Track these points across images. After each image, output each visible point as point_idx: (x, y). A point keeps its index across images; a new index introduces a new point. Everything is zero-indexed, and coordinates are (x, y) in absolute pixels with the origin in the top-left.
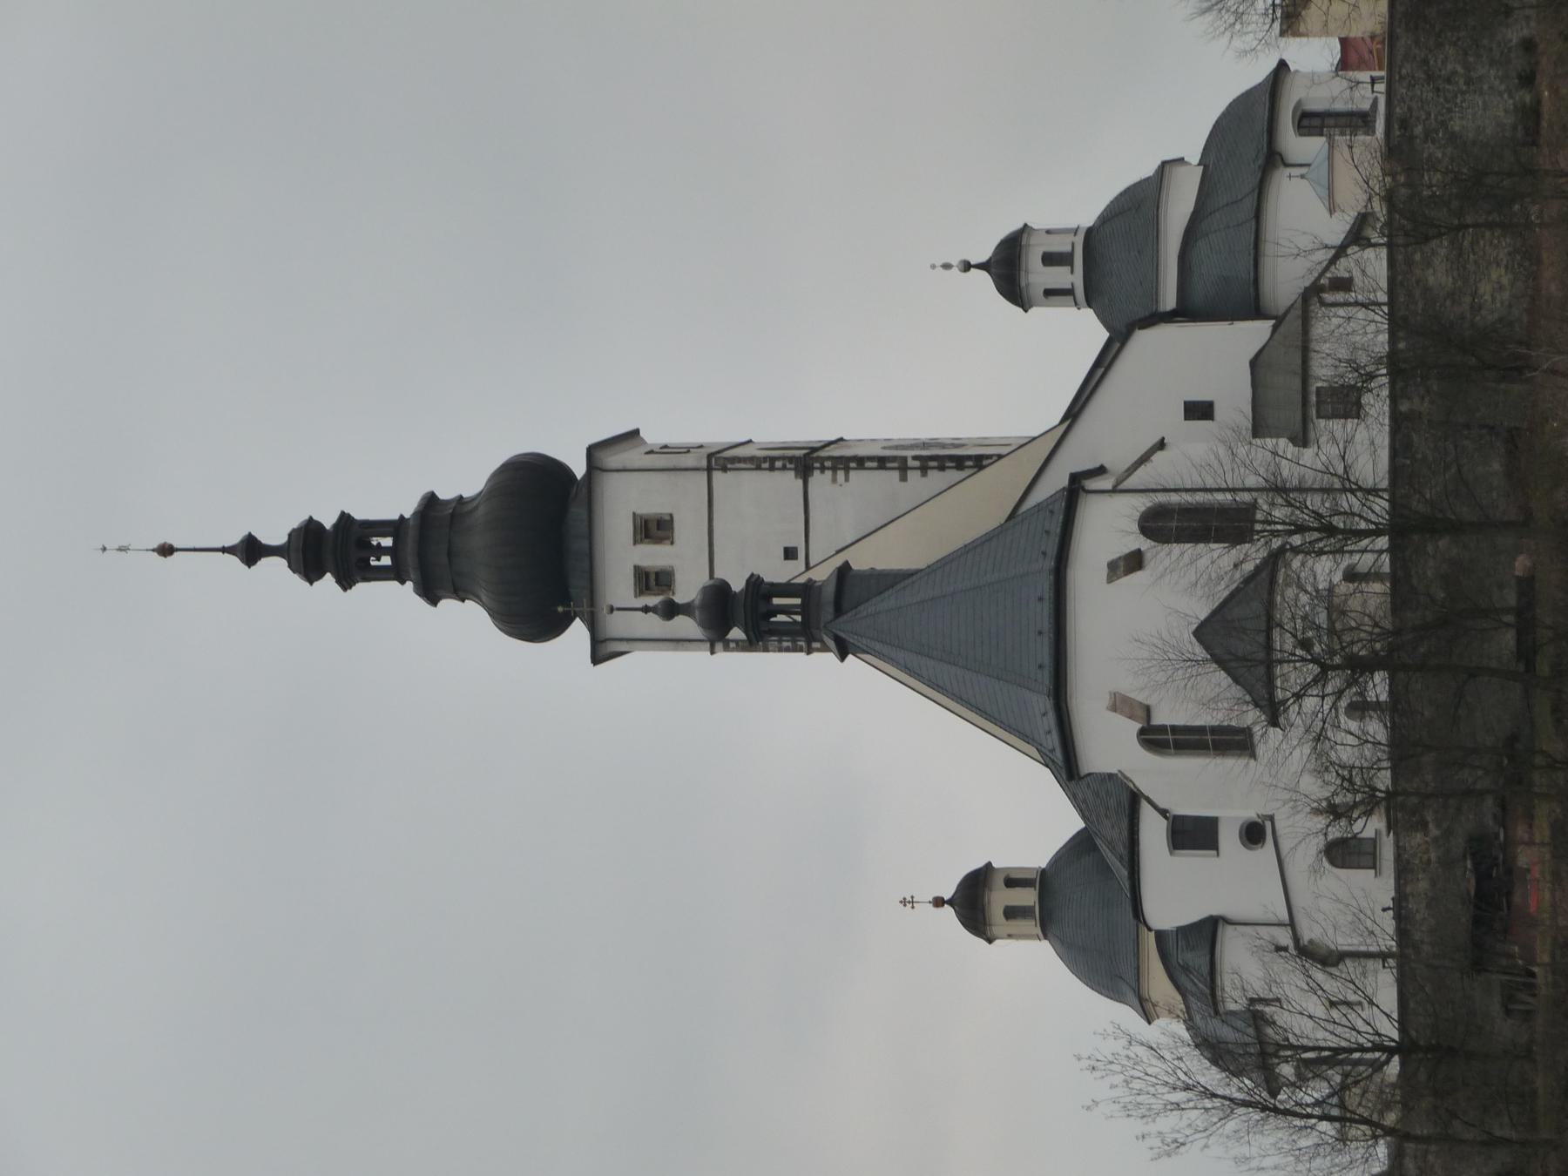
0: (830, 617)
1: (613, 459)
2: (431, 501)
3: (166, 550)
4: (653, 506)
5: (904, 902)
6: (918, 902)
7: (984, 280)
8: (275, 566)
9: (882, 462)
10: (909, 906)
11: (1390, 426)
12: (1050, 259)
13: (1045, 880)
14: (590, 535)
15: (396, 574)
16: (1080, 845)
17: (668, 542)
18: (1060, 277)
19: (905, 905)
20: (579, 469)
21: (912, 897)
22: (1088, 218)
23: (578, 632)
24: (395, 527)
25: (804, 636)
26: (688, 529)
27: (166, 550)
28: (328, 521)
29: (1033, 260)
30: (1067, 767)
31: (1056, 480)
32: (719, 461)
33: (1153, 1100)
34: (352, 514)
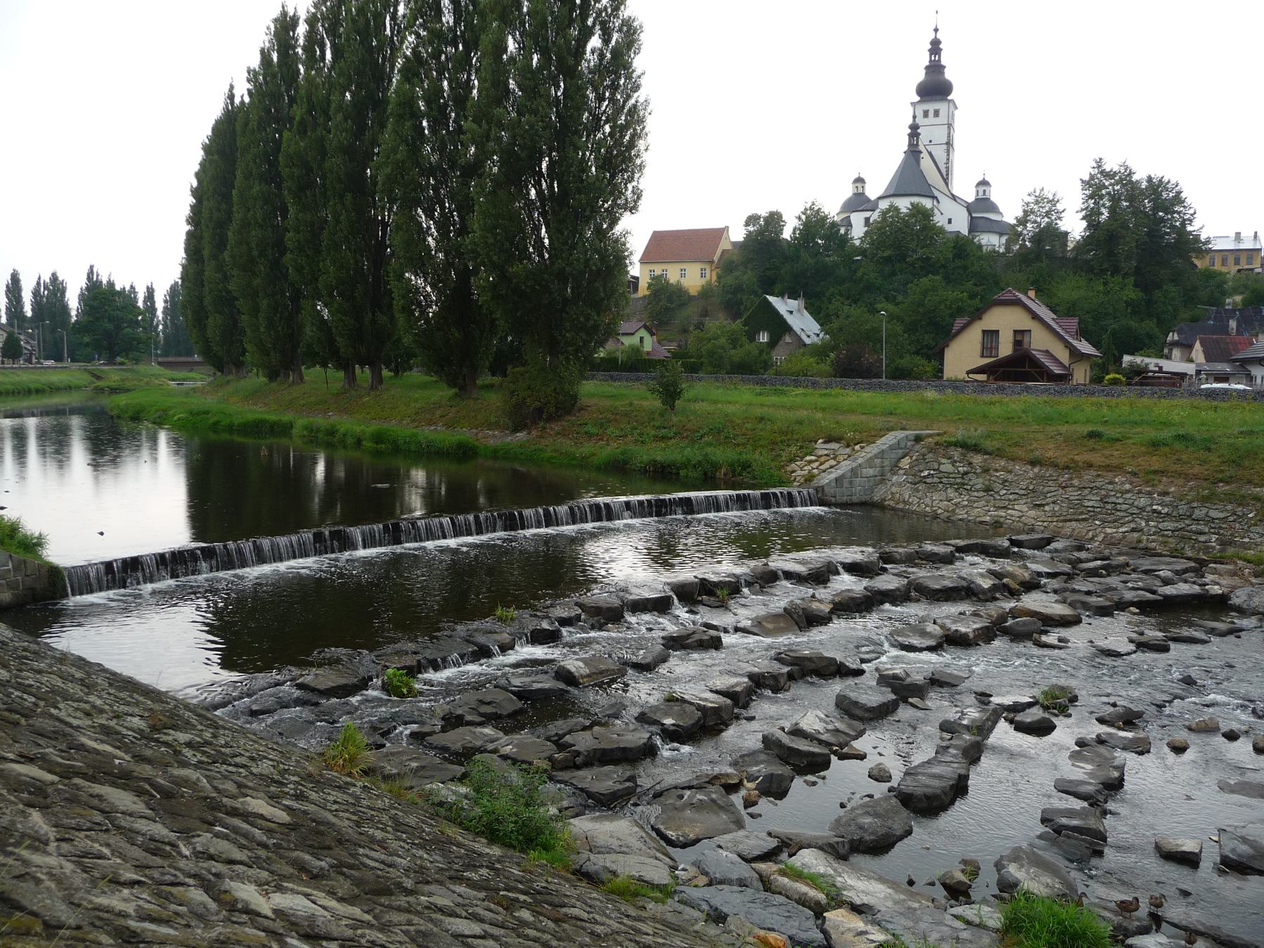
4: (941, 113)
7: (981, 179)
8: (933, 36)
9: (948, 159)
14: (936, 100)
15: (931, 61)
16: (868, 200)
18: (981, 193)
20: (949, 98)
22: (992, 199)
23: (918, 99)
24: (939, 60)
25: (910, 145)
26: (937, 121)
29: (984, 188)
32: (950, 126)
33: (1245, 653)
34: (187, 211)
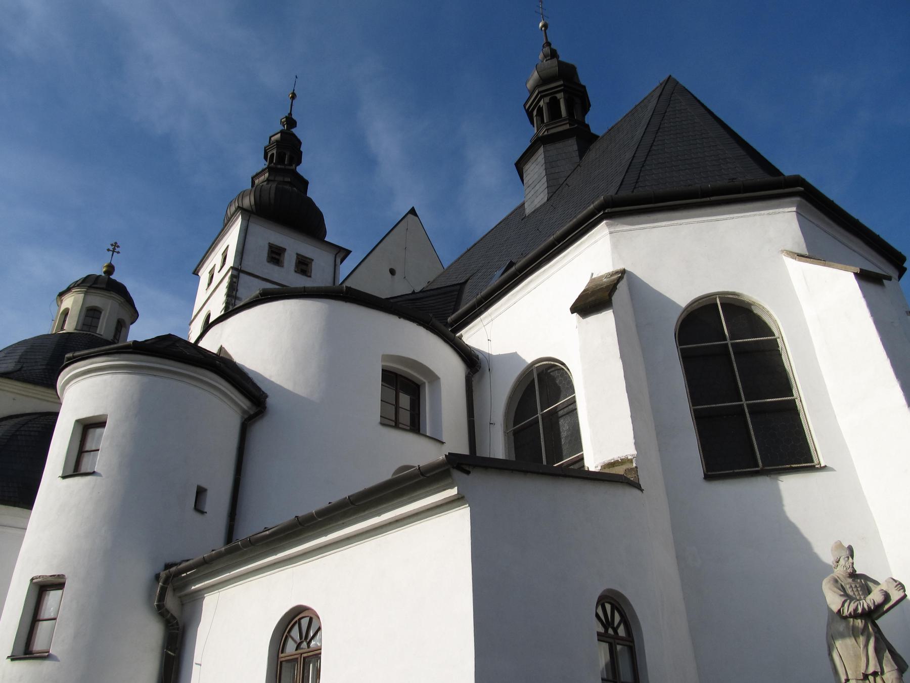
0: (217, 307)
3: (294, 96)
5: (115, 245)
6: (112, 255)
10: (111, 248)
17: (296, 270)
19: (112, 245)
21: (118, 252)
28: (905, 265)
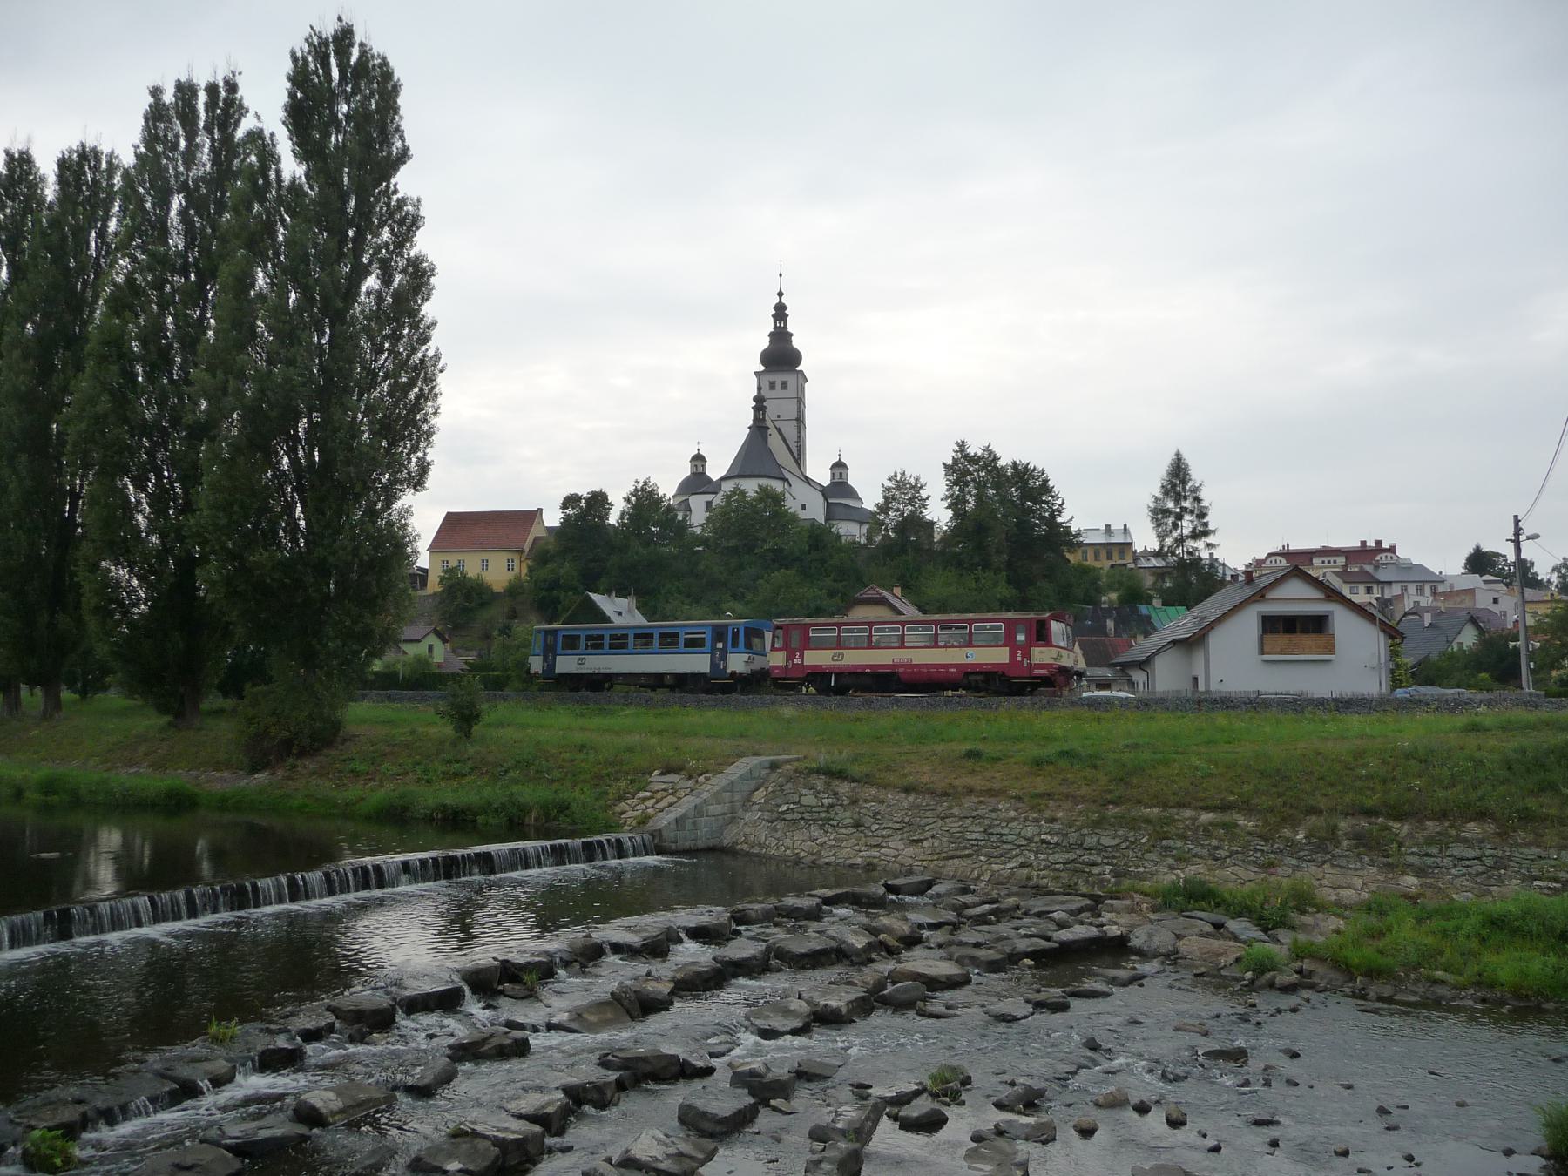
1: (800, 377)
2: (792, 335)
3: (781, 275)
9: (799, 437)
11: (21, 913)
12: (841, 474)
13: (703, 473)
15: (775, 327)
16: (709, 480)
20: (798, 369)
23: (763, 368)
27: (781, 275)
28: (787, 312)
30: (723, 479)
31: (787, 475)
